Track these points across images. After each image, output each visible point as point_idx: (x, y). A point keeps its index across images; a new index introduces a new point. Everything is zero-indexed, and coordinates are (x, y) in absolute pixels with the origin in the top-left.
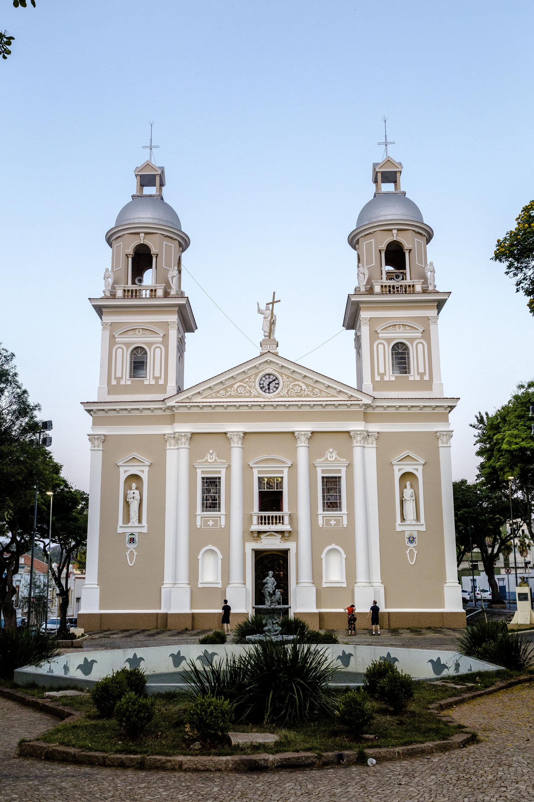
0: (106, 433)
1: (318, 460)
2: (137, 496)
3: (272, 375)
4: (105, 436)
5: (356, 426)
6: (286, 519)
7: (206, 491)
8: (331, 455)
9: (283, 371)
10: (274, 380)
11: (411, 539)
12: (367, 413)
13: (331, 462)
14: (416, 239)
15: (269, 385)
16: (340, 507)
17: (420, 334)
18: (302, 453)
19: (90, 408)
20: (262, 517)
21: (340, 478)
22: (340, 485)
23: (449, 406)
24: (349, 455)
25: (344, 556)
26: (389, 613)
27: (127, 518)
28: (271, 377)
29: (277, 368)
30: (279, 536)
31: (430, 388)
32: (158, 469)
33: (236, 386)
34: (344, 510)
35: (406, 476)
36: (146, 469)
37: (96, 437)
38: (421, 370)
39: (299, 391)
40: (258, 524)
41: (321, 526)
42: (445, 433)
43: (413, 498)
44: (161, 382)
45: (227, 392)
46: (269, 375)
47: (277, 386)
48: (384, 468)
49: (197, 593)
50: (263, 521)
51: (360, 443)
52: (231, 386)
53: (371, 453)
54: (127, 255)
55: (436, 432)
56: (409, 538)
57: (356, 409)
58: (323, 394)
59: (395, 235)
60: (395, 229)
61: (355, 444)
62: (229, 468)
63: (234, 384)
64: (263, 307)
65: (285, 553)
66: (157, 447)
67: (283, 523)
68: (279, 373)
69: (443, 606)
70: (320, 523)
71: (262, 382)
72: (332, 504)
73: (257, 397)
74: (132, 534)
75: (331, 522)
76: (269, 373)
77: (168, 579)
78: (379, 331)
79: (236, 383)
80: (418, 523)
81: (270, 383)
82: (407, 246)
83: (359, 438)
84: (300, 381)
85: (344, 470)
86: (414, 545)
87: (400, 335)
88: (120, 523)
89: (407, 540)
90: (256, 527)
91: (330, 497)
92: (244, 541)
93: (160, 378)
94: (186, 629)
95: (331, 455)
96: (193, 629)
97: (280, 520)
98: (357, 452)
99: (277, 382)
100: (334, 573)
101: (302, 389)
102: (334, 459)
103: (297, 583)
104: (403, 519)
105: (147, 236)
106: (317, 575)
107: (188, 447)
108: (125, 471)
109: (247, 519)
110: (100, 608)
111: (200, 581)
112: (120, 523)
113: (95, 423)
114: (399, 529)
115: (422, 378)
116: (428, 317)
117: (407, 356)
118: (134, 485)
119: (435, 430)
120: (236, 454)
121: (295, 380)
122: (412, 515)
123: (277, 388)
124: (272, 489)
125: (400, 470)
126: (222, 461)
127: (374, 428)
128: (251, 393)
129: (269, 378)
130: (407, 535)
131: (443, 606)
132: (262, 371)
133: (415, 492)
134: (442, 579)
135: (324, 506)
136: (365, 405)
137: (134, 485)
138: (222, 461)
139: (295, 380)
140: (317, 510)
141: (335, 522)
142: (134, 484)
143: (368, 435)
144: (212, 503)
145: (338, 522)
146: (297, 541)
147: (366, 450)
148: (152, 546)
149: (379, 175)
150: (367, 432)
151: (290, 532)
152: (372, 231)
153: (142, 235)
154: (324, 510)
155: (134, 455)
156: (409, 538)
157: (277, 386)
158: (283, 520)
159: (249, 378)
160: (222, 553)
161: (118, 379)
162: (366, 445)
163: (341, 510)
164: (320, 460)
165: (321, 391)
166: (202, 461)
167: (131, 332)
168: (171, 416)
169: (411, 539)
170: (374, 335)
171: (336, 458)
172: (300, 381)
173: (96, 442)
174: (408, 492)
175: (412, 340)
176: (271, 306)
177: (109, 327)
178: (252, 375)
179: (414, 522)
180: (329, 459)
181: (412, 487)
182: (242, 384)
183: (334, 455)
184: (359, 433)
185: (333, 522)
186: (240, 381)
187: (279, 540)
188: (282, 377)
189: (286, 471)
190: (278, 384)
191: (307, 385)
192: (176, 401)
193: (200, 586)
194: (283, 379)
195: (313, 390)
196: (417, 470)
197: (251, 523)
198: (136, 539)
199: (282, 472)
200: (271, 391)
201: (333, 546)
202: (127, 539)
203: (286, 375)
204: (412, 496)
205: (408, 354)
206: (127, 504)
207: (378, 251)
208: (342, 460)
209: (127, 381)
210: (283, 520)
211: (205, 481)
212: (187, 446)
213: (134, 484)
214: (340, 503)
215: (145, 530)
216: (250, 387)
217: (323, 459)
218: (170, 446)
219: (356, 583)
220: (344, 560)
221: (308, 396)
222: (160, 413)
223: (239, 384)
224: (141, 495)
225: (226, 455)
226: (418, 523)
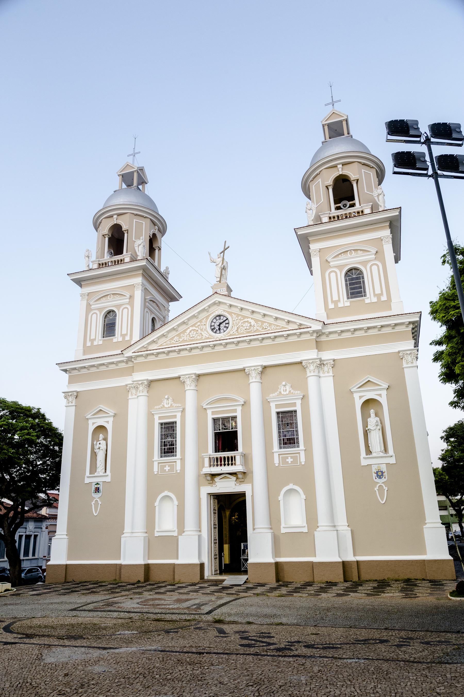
0: (78, 390)
1: (271, 395)
2: (103, 446)
3: (222, 316)
5: (309, 355)
6: (238, 460)
7: (163, 436)
8: (285, 389)
9: (233, 310)
10: (225, 321)
11: (380, 474)
12: (319, 340)
13: (285, 396)
14: (363, 170)
15: (219, 325)
16: (298, 443)
17: (374, 256)
18: (255, 389)
19: (67, 368)
20: (217, 458)
22: (296, 420)
23: (410, 323)
24: (302, 385)
25: (304, 497)
26: (357, 562)
28: (222, 317)
29: (226, 308)
30: (234, 478)
32: (121, 418)
33: (188, 331)
35: (368, 403)
36: (111, 420)
37: (70, 394)
38: (378, 291)
39: (248, 328)
40: (210, 466)
41: (277, 465)
42: (409, 352)
43: (380, 427)
44: (127, 338)
45: (180, 337)
46: (219, 316)
47: (227, 325)
48: (343, 398)
49: (153, 542)
50: (219, 463)
51: (314, 372)
52: (184, 331)
53: (328, 383)
54: (103, 235)
56: (377, 473)
57: (307, 337)
59: (340, 169)
60: (339, 164)
61: (309, 374)
62: (183, 411)
63: (187, 329)
64: (215, 256)
65: (243, 495)
66: (120, 397)
67: (235, 464)
68: (229, 313)
69: (425, 553)
70: (276, 461)
71: (213, 324)
72: (289, 441)
73: (208, 338)
74: (98, 484)
75: (287, 460)
77: (127, 529)
78: (329, 260)
79: (189, 328)
80: (386, 455)
81: (221, 323)
82: (353, 177)
83: (312, 367)
84: (250, 318)
85: (299, 402)
86: (383, 480)
87: (352, 261)
88: (88, 473)
89: (375, 475)
91: (285, 433)
92: (199, 485)
94: (139, 582)
95: (285, 389)
96: (145, 581)
97: (231, 461)
98: (312, 382)
99: (227, 322)
100: (294, 517)
101: (251, 325)
102: (287, 392)
103: (254, 529)
104: (369, 451)
105: (120, 217)
106: (274, 518)
107: (147, 394)
108: (93, 423)
109: (200, 464)
110: (69, 559)
111: (157, 529)
112: (88, 473)
113: (71, 381)
114: (364, 462)
115: (379, 298)
116: (380, 238)
117: (361, 280)
118: (101, 436)
120: (190, 396)
122: (379, 447)
123: (227, 328)
124: (227, 429)
125: (360, 397)
126: (177, 405)
127: (327, 355)
128: (202, 335)
129: (220, 319)
130: (374, 469)
132: (212, 313)
133: (380, 420)
134: (421, 518)
135: (280, 444)
136: (314, 331)
137: (101, 436)
138: (177, 405)
139: (245, 317)
140: (272, 448)
141: (292, 460)
142: (101, 435)
143: (322, 364)
144: (168, 449)
145: (295, 459)
146: (252, 482)
147: (322, 380)
148: (113, 495)
149: (326, 128)
150: (321, 360)
151: (244, 473)
152: (318, 172)
153: (115, 217)
154: (280, 448)
155: (100, 407)
156: (377, 473)
157: (227, 325)
158: (235, 460)
159: (201, 321)
160: (178, 499)
161: (92, 341)
162: (321, 375)
164: (274, 395)
165: (270, 324)
166: (159, 406)
167: (104, 299)
169: (380, 474)
170: (325, 264)
171: (290, 391)
172: (250, 318)
173: (70, 399)
174: (373, 421)
175: (364, 263)
176: (222, 254)
177: (86, 297)
178: (203, 319)
179: (382, 454)
180: (283, 393)
181: (376, 415)
182: (194, 328)
183: (288, 388)
184: (311, 361)
185: (290, 460)
186: (192, 326)
187: (234, 483)
188: (231, 316)
189: (239, 409)
190: (228, 323)
192: (133, 351)
193: (157, 534)
194: (232, 318)
195: (262, 324)
196: (380, 395)
197: (203, 466)
198: (101, 489)
199: (235, 411)
200: (222, 331)
201: (291, 486)
202: (93, 489)
203: (235, 314)
204: (377, 425)
205: (363, 278)
207: (325, 188)
208: (296, 392)
209: (99, 341)
210: (235, 460)
211: (163, 426)
212: (145, 393)
213: (101, 435)
214: (298, 438)
215: (108, 479)
216: (202, 330)
217: (276, 394)
218: (132, 395)
219: (184, 532)
220: (303, 502)
222: (123, 365)
223: (191, 329)
226: (386, 455)
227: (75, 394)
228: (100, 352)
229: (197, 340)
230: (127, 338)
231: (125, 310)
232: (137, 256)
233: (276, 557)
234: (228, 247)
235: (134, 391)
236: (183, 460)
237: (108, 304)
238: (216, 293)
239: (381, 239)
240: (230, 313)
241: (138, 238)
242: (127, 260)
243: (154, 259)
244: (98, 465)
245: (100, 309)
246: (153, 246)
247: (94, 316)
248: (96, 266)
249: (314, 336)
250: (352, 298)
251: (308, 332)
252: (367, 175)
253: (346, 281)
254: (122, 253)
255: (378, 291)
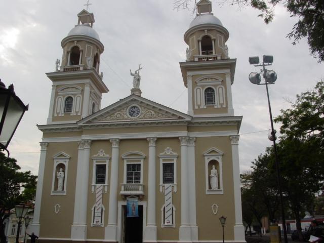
0: (49, 141)
1: (94, 155)
2: (63, 176)
4: (196, 138)
5: (183, 133)
17: (220, 83)
21: (173, 164)
24: (178, 150)
27: (56, 188)
30: (138, 198)
31: (227, 112)
32: (73, 160)
33: (116, 114)
34: (175, 183)
38: (221, 102)
43: (217, 175)
53: (191, 151)
55: (230, 136)
58: (164, 116)
62: (110, 159)
66: (74, 149)
76: (135, 101)
78: (197, 82)
82: (81, 48)
83: (184, 141)
87: (209, 84)
90: (123, 192)
93: (223, 104)
98: (183, 149)
103: (147, 225)
104: (210, 187)
109: (119, 189)
113: (45, 136)
118: (61, 169)
119: (229, 135)
120: (115, 152)
121: (148, 109)
125: (208, 158)
127: (194, 135)
131: (70, 237)
136: (187, 121)
140: (159, 182)
144: (101, 179)
150: (189, 137)
163: (173, 183)
168: (80, 130)
174: (214, 171)
175: (216, 86)
181: (216, 168)
186: (119, 111)
191: (155, 112)
192: (84, 122)
197: (121, 190)
205: (214, 93)
206: (57, 180)
221: (155, 117)
224: (218, 172)
225: (109, 152)
227: (47, 144)
228: (210, 114)
229: (121, 119)
230: (79, 114)
231: (79, 98)
232: (87, 66)
233: (87, 238)
234: (142, 68)
235: (81, 145)
236: (109, 186)
237: (69, 93)
238: (134, 94)
239: (225, 74)
240: (141, 106)
241: (88, 55)
242: (81, 68)
243: (96, 68)
244: (59, 186)
245: (64, 96)
246: (96, 60)
247: (60, 99)
248: (62, 70)
249: (186, 124)
250: (207, 104)
251: (183, 122)
252: (220, 37)
253: (205, 94)
254: (78, 64)
255: (199, 103)
